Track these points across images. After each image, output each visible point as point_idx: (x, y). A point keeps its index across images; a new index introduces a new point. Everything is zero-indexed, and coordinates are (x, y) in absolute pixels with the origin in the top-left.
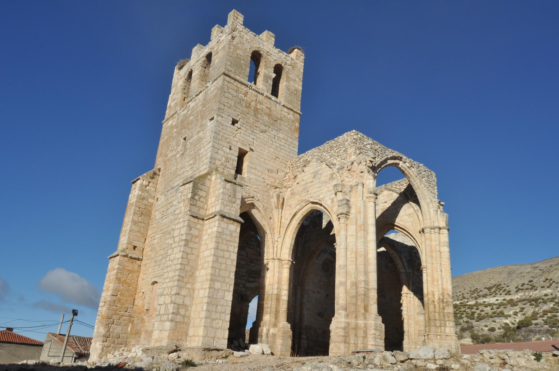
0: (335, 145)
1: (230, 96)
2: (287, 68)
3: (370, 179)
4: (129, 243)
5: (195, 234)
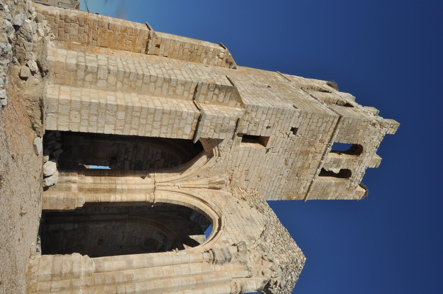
0: (285, 239)
1: (319, 125)
2: (347, 182)
3: (257, 284)
4: (162, 40)
5: (177, 91)
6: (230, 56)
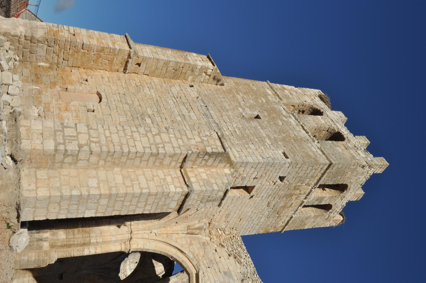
1: (308, 172)
2: (327, 214)
4: (144, 59)
6: (218, 73)
